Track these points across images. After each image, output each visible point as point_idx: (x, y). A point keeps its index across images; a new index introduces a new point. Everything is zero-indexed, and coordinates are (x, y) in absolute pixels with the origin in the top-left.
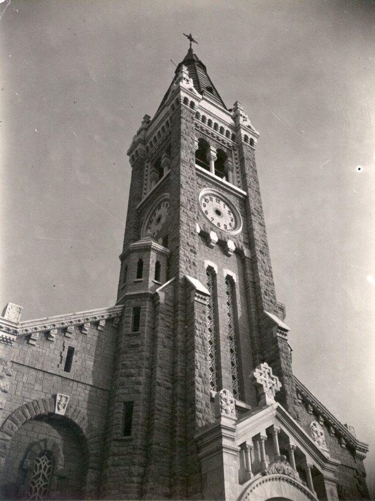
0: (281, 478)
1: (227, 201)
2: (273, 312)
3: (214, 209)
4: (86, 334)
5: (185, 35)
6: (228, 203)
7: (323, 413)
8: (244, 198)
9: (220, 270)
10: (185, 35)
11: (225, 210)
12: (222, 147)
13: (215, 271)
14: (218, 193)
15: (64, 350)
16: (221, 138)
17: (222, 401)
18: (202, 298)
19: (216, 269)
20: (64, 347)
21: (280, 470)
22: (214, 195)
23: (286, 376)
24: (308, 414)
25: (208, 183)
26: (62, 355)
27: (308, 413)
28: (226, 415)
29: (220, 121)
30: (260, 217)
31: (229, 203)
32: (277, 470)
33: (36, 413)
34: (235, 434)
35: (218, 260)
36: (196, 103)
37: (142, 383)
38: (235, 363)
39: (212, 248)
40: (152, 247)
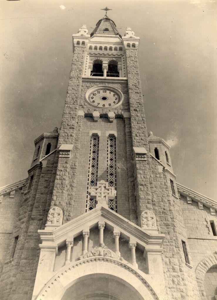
0: (97, 259)
2: (143, 145)
8: (125, 82)
9: (104, 133)
12: (113, 58)
13: (115, 136)
18: (65, 154)
21: (95, 254)
22: (102, 89)
23: (141, 186)
24: (199, 210)
26: (208, 227)
30: (137, 89)
32: (92, 253)
33: (208, 267)
34: (54, 236)
35: (102, 127)
38: (184, 192)
39: (97, 122)
40: (44, 136)
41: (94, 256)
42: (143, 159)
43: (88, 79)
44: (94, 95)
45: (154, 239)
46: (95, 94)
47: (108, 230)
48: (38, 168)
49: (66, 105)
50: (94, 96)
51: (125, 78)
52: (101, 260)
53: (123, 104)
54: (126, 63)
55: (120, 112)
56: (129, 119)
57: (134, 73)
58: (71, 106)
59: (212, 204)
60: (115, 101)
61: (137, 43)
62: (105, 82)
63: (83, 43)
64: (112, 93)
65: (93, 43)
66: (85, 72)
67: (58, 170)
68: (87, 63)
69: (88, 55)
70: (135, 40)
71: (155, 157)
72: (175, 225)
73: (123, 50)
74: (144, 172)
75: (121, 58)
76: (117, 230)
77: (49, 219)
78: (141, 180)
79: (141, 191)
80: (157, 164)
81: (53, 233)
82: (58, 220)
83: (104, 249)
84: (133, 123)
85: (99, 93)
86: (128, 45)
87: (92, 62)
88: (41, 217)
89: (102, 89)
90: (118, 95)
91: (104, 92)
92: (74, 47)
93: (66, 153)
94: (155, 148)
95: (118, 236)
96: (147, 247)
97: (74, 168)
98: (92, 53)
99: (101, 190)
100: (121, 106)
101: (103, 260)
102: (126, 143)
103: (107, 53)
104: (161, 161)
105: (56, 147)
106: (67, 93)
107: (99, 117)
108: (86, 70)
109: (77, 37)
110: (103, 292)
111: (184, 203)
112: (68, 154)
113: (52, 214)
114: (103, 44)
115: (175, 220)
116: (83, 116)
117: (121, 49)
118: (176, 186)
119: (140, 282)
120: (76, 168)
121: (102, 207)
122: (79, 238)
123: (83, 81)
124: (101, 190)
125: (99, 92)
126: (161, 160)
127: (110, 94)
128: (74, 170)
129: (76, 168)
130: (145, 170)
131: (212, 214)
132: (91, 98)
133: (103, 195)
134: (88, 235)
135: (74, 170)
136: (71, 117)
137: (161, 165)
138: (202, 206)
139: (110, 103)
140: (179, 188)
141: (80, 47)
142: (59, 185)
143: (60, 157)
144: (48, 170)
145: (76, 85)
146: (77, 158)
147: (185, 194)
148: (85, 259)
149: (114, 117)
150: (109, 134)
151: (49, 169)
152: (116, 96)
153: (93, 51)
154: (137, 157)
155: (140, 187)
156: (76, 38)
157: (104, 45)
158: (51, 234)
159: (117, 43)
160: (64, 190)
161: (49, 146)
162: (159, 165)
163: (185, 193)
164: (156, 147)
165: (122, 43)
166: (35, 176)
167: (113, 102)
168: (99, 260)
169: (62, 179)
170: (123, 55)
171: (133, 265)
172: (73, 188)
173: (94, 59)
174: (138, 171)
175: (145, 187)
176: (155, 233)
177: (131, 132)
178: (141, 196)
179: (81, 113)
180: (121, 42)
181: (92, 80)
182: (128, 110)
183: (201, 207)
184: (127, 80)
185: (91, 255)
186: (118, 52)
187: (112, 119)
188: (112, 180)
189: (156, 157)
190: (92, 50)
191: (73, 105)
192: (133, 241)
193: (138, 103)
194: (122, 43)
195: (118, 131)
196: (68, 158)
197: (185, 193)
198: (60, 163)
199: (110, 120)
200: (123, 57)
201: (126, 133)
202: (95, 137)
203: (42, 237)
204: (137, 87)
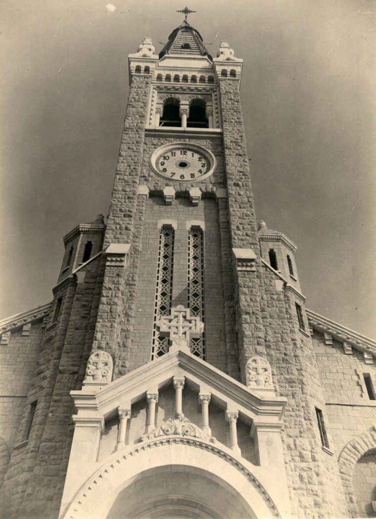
1: (195, 148)
2: (249, 245)
3: (189, 163)
4: (7, 345)
5: (194, 12)
6: (197, 150)
7: (369, 348)
8: (219, 136)
10: (194, 12)
11: (192, 158)
13: (202, 229)
14: (172, 145)
15: (360, 379)
17: (250, 371)
18: (117, 261)
19: (175, 226)
20: (358, 375)
22: (178, 149)
23: (246, 314)
24: (344, 356)
25: (168, 139)
27: (345, 354)
28: (258, 387)
29: (171, 70)
30: (240, 148)
31: (198, 150)
32: (163, 431)
34: (97, 401)
36: (152, 66)
37: (48, 376)
40: (80, 229)
41: (166, 435)
42: (249, 269)
43: (155, 131)
44: (165, 158)
45: (268, 405)
46: (167, 158)
47: (190, 391)
48: (71, 283)
49: (118, 177)
51: (219, 130)
52: (178, 441)
53: (214, 175)
54: (220, 103)
56: (226, 200)
57: (233, 121)
58: (126, 178)
60: (201, 170)
61: (238, 70)
62: (184, 137)
63: (147, 69)
64: (197, 156)
65: (164, 70)
66: (150, 119)
67: (103, 288)
69: (154, 90)
70: (236, 64)
72: (304, 383)
73: (215, 82)
74: (252, 291)
75: (211, 95)
76: (206, 391)
77: (90, 373)
78: (246, 304)
79: (247, 323)
80: (274, 276)
81: (96, 396)
82: (104, 373)
83: (183, 423)
84: (233, 207)
85: (175, 156)
86: (224, 73)
88: (75, 369)
89: (178, 149)
90: (205, 158)
91: (183, 153)
92: (131, 76)
93: (119, 259)
94: (270, 249)
95: (208, 400)
96: (257, 419)
97: (132, 285)
98: (162, 86)
99: (177, 322)
100: (212, 178)
101: (182, 441)
102: (220, 242)
104: (280, 273)
106: (120, 155)
107: (174, 196)
109: (136, 59)
110: (181, 496)
111: (319, 344)
112: (121, 261)
113: (95, 363)
114: (181, 70)
115: (304, 373)
116: (146, 195)
117: (211, 80)
118: (306, 315)
119: (244, 479)
120: (135, 285)
121: (180, 351)
122: (141, 404)
123: (146, 136)
124: (177, 322)
125: (175, 153)
126: (279, 271)
127: (193, 156)
128: (132, 288)
129: (135, 285)
130: (253, 287)
131: (367, 362)
133: (181, 331)
134: (155, 399)
135: (132, 288)
136: (127, 197)
137: (281, 279)
138: (350, 349)
140: (311, 318)
141: (141, 76)
142: (106, 314)
143: (108, 266)
145: (135, 142)
146: (136, 267)
147: (321, 328)
148: (150, 441)
149: (199, 197)
152: (203, 161)
153: (164, 83)
154: (239, 266)
155: (244, 316)
156: (134, 61)
158: (92, 397)
159: (206, 70)
160: (115, 322)
161: (88, 247)
162: (277, 279)
163: (321, 326)
164: (271, 248)
165: (213, 69)
168: (175, 441)
169: (112, 303)
170: (215, 89)
171: (232, 449)
173: (166, 96)
174: (241, 288)
175: (254, 317)
176: (270, 396)
177: (228, 222)
178: (246, 333)
179: (144, 190)
180: (212, 67)
181: (161, 133)
183: (348, 350)
184: (221, 134)
185: (162, 433)
186: (206, 85)
187: (196, 199)
189: (272, 266)
191: (129, 177)
192: (233, 408)
193: (241, 172)
194: (213, 69)
195: (207, 221)
196: (121, 268)
197: (321, 326)
198: (108, 276)
199: (194, 201)
200: (215, 93)
201: (221, 224)
202: (168, 230)
203: (78, 403)
204: (239, 146)
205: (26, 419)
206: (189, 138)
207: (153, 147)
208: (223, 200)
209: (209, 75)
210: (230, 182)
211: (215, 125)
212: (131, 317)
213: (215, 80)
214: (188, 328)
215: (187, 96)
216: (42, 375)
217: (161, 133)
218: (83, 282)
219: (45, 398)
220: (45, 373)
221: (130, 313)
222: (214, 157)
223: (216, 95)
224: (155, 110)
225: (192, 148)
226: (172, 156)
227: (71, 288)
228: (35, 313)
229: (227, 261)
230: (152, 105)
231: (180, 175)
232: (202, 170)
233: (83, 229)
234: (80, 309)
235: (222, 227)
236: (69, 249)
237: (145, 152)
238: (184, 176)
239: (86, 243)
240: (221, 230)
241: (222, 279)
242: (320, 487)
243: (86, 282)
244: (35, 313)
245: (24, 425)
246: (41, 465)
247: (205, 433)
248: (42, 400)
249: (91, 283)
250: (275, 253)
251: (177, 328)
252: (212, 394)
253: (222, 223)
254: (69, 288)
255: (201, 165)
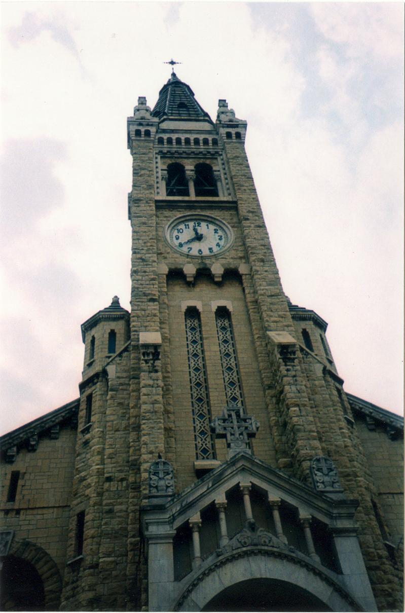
13: (228, 310)
16: (181, 150)
19: (200, 307)
46: (181, 231)
50: (179, 234)
54: (229, 168)
55: (233, 264)
59: (359, 406)
60: (218, 243)
66: (158, 188)
68: (158, 170)
69: (157, 155)
71: (304, 347)
75: (217, 159)
85: (188, 228)
87: (165, 167)
88: (122, 475)
102: (250, 324)
103: (160, 149)
104: (316, 355)
105: (128, 337)
108: (158, 185)
118: (347, 399)
125: (188, 225)
126: (316, 353)
127: (208, 228)
128: (167, 381)
132: (174, 239)
133: (237, 433)
137: (321, 363)
139: (211, 247)
141: (142, 140)
144: (121, 384)
150: (216, 308)
151: (122, 381)
153: (166, 148)
157: (193, 135)
164: (304, 328)
166: (96, 395)
167: (217, 245)
172: (169, 415)
173: (169, 161)
182: (246, 258)
188: (233, 395)
189: (307, 347)
190: (164, 145)
200: (221, 157)
201: (249, 304)
202: (192, 313)
205: (74, 532)
206: (202, 208)
207: (165, 219)
208: (247, 276)
209: (213, 137)
210: (253, 258)
211: (226, 193)
212: (170, 413)
213: (219, 142)
214: (244, 428)
215: (191, 160)
216: (84, 483)
217: (228, 205)
218: (114, 377)
219: (93, 508)
220: (89, 481)
221: (169, 409)
222: (230, 228)
223: (222, 160)
224: (160, 178)
225: (206, 218)
226: (186, 228)
227: (101, 383)
228: (62, 412)
229: (261, 345)
230: (157, 172)
231: (198, 249)
232: (220, 244)
233: (104, 316)
234: (117, 408)
235: (251, 307)
236: (89, 339)
237: (158, 225)
238: (202, 250)
239: (109, 331)
240: (251, 310)
241: (258, 365)
242: (389, 585)
243: (118, 377)
244: (62, 412)
245: (74, 539)
246: (104, 584)
247: (281, 541)
248: (91, 511)
249: (123, 378)
250: (308, 332)
251: (232, 428)
252: (281, 499)
253: (250, 302)
254: (99, 384)
255: (218, 238)
